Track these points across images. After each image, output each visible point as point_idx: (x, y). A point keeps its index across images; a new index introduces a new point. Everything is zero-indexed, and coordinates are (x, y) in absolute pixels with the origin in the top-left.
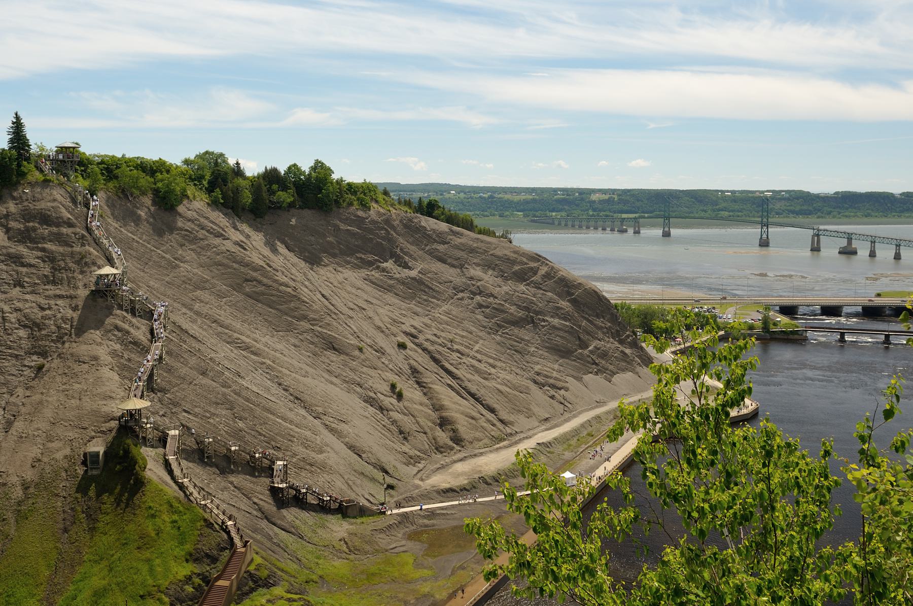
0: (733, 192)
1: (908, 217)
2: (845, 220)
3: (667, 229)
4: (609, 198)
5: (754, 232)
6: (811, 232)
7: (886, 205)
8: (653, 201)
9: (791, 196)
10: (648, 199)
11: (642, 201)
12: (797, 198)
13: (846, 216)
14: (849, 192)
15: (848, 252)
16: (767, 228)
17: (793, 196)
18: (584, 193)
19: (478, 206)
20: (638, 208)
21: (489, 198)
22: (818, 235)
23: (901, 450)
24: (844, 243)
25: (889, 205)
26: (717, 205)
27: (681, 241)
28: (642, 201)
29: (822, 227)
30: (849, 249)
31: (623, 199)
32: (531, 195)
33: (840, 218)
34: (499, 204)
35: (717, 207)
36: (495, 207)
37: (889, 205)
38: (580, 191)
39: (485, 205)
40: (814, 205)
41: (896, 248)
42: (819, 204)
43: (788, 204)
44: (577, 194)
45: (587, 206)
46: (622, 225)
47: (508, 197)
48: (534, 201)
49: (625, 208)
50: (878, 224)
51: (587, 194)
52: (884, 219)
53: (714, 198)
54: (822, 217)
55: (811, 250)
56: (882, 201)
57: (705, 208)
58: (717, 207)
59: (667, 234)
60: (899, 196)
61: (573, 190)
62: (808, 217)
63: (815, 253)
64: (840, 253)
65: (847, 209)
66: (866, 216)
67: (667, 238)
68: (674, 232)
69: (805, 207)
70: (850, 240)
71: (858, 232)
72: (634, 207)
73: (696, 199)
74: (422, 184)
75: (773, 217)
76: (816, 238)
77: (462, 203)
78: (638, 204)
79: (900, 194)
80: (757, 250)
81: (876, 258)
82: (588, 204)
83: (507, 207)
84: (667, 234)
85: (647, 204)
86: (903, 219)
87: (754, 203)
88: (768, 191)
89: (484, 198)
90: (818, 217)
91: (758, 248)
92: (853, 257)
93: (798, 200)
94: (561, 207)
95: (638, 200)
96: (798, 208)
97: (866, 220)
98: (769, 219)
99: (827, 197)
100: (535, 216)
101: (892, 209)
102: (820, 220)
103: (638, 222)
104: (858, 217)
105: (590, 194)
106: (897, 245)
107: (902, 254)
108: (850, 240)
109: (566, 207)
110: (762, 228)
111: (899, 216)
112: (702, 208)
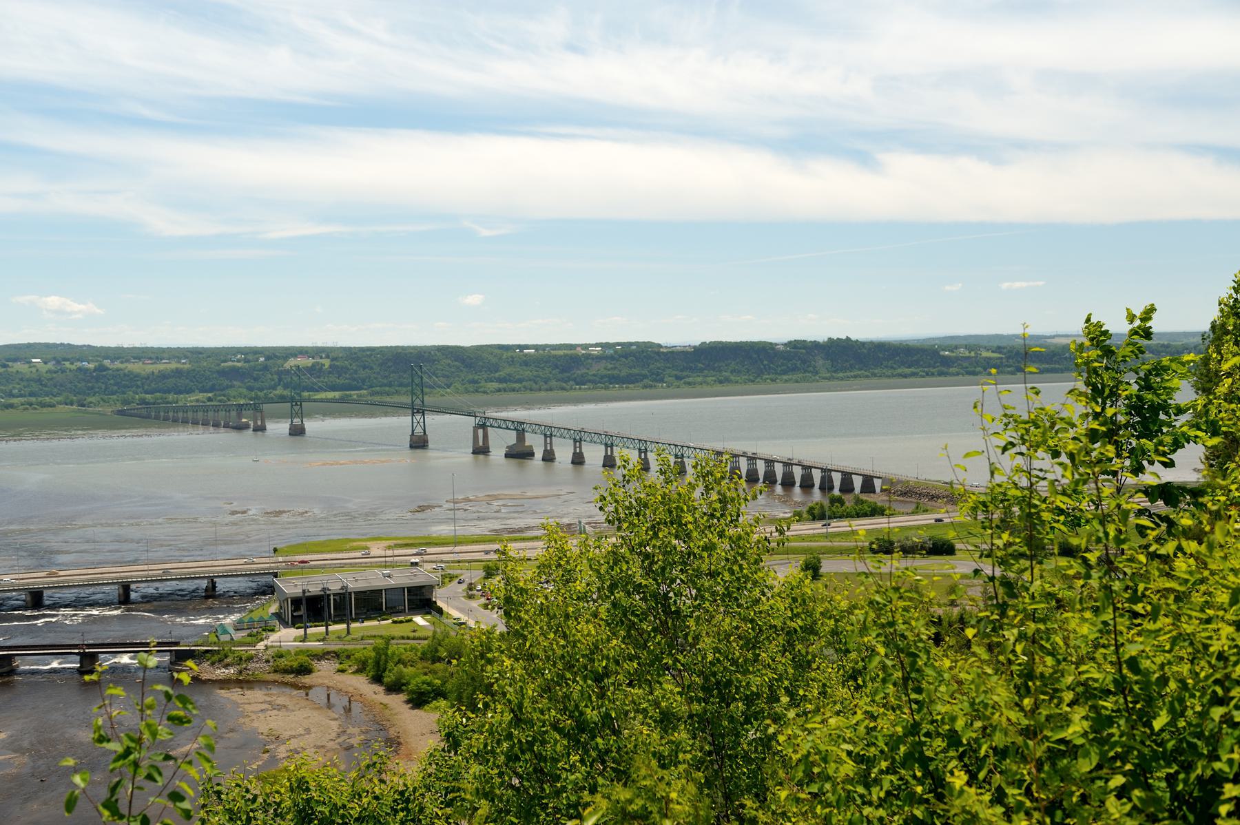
0: (605, 346)
1: (786, 381)
2: (687, 389)
3: (297, 421)
4: (313, 365)
5: (402, 423)
6: (471, 421)
7: (762, 362)
8: (389, 367)
9: (616, 352)
10: (381, 365)
11: (371, 368)
12: (626, 356)
13: (689, 384)
14: (721, 343)
15: (520, 454)
16: (423, 415)
17: (620, 352)
18: (276, 355)
19: (69, 385)
20: (364, 381)
21: (95, 370)
22: (484, 426)
23: (796, 748)
24: (511, 438)
25: (765, 362)
26: (496, 372)
27: (328, 443)
28: (371, 368)
29: (492, 413)
30: (519, 449)
31: (337, 366)
32: (179, 362)
33: (678, 387)
34: (112, 382)
35: (497, 375)
36: (103, 386)
37: (765, 362)
38: (267, 353)
39: (83, 384)
40: (651, 366)
41: (546, 440)
42: (658, 365)
43: (610, 366)
44: (262, 359)
45: (273, 380)
46: (240, 416)
47: (135, 367)
48: (178, 373)
49: (341, 381)
50: (753, 394)
51: (279, 358)
52: (750, 386)
53: (494, 360)
54: (651, 386)
55: (474, 453)
56: (755, 356)
57: (476, 377)
58: (497, 375)
59: (297, 431)
60: (782, 348)
61: (256, 352)
62: (627, 388)
63: (481, 457)
64: (507, 456)
65: (702, 370)
66: (721, 382)
67: (298, 438)
68: (312, 426)
69: (635, 371)
70: (521, 434)
71: (533, 420)
72: (354, 380)
73: (463, 361)
74: (414, 348)
75: (571, 389)
76: (480, 432)
77: (39, 381)
78: (363, 373)
79: (785, 345)
80: (407, 458)
81: (585, 466)
82: (276, 377)
83: (126, 386)
84: (297, 431)
85: (378, 373)
86: (780, 385)
87: (556, 367)
88: (597, 345)
89: (87, 370)
90: (645, 387)
91: (410, 451)
92: (528, 462)
93: (626, 358)
94: (226, 382)
95: (364, 368)
96: (624, 372)
97: (718, 388)
98: (426, 398)
99: (672, 352)
100: (125, 402)
101: (770, 368)
102: (647, 391)
103: (261, 411)
104: (708, 384)
105: (286, 358)
106: (575, 441)
107: (585, 455)
108: (521, 434)
109: (235, 383)
110: (413, 415)
111: (772, 380)
112: (471, 377)
